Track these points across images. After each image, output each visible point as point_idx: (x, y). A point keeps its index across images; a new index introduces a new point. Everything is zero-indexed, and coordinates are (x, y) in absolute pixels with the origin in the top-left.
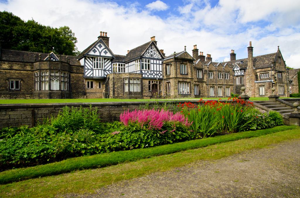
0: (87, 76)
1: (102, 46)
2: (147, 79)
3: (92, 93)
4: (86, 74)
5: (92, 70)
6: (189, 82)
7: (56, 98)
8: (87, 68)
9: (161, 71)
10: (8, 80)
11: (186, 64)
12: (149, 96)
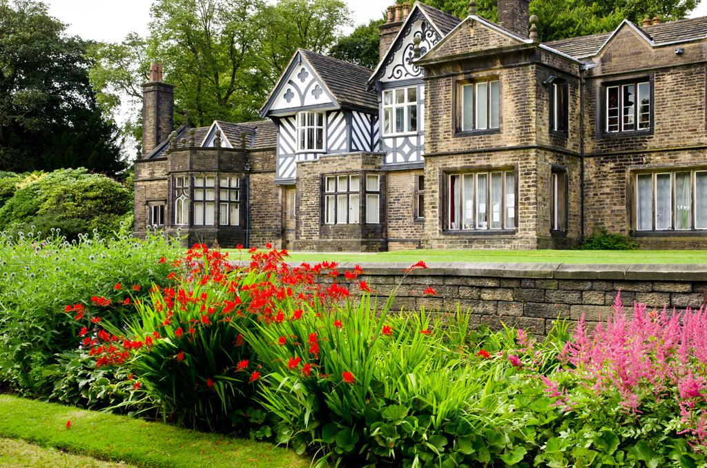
0: (283, 177)
2: (409, 171)
4: (281, 171)
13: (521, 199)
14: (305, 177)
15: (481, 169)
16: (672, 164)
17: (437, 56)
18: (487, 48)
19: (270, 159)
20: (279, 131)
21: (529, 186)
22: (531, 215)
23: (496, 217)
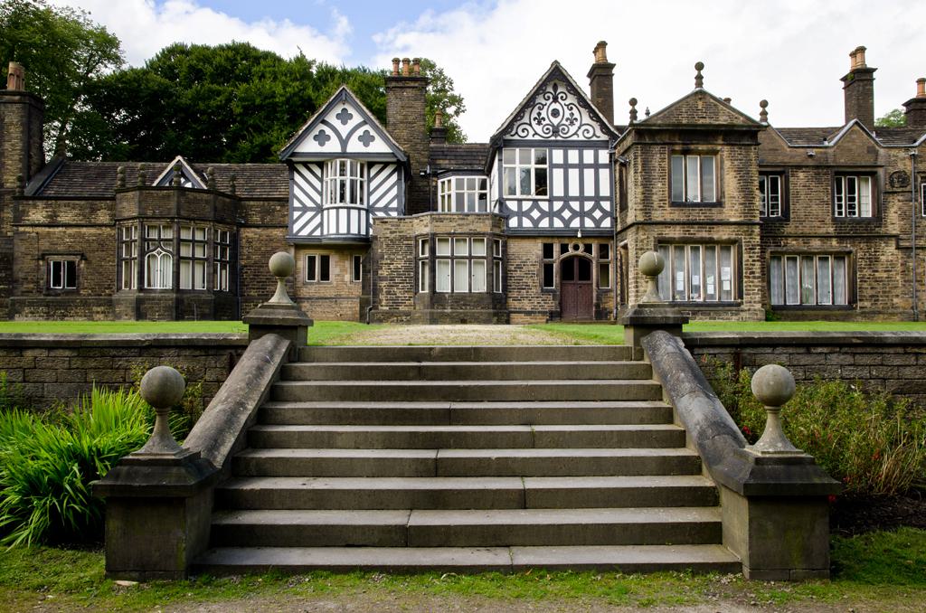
1: (351, 116)
3: (322, 298)
4: (296, 227)
5: (320, 209)
6: (734, 242)
7: (158, 319)
8: (300, 206)
9: (605, 199)
10: (43, 259)
11: (715, 153)
12: (544, 313)
13: (746, 273)
14: (388, 235)
15: (703, 241)
16: (806, 249)
17: (659, 122)
18: (717, 123)
19: (274, 210)
20: (293, 179)
21: (754, 261)
22: (757, 289)
23: (711, 290)
